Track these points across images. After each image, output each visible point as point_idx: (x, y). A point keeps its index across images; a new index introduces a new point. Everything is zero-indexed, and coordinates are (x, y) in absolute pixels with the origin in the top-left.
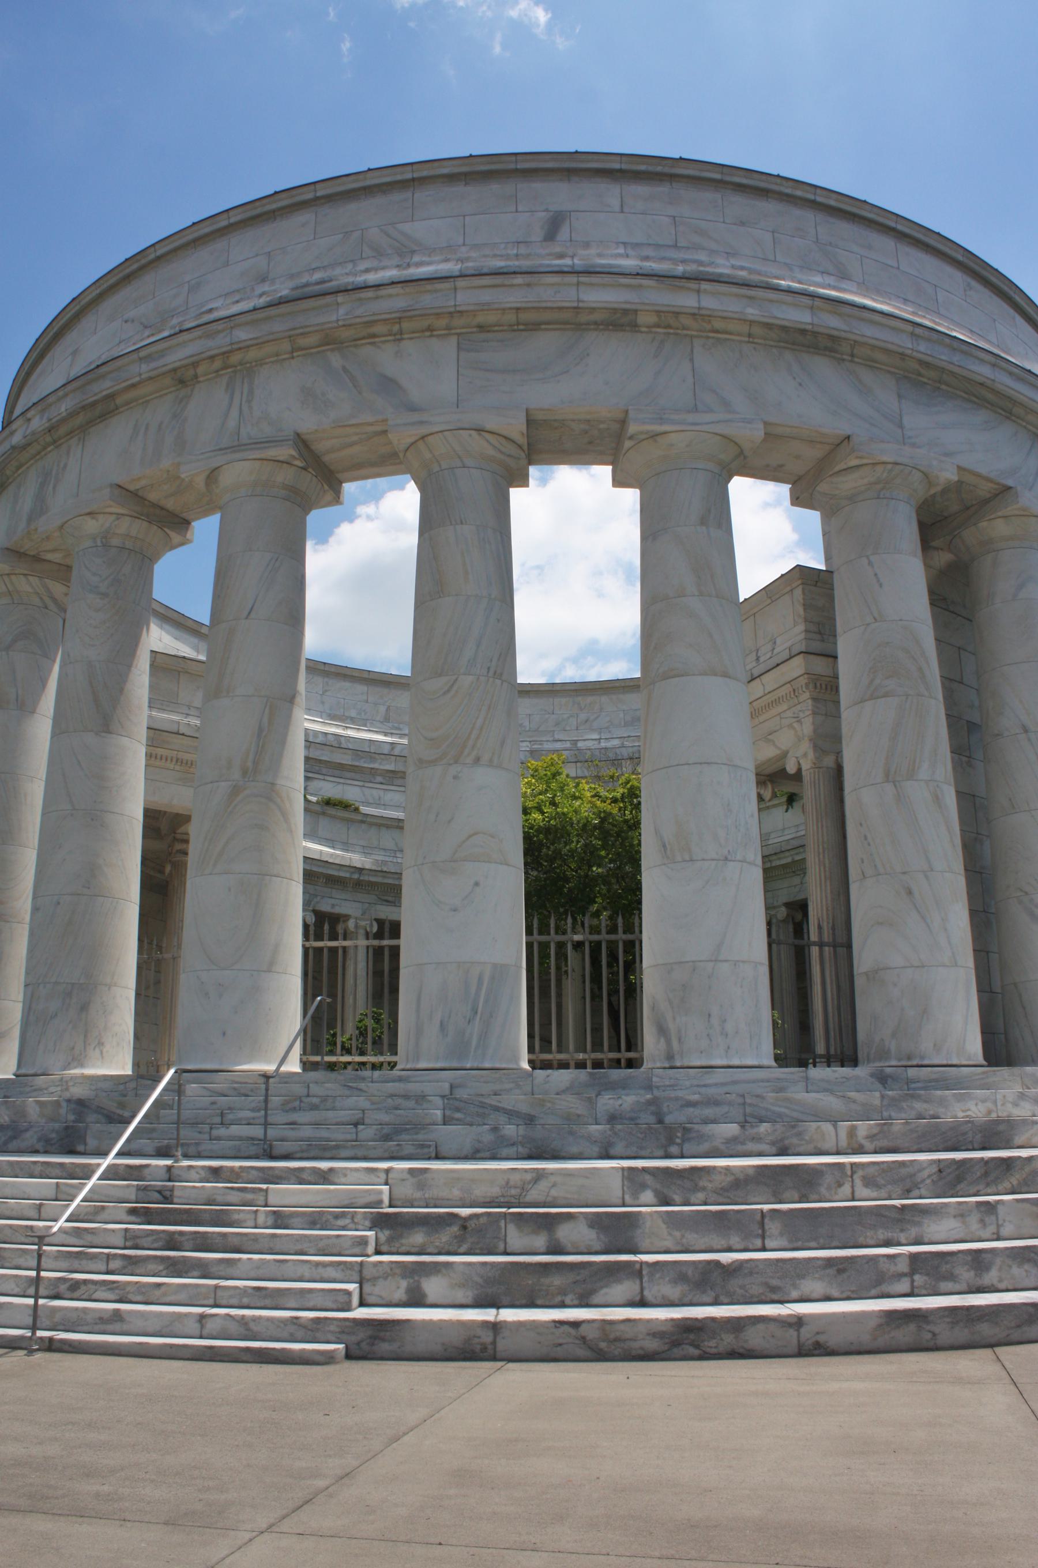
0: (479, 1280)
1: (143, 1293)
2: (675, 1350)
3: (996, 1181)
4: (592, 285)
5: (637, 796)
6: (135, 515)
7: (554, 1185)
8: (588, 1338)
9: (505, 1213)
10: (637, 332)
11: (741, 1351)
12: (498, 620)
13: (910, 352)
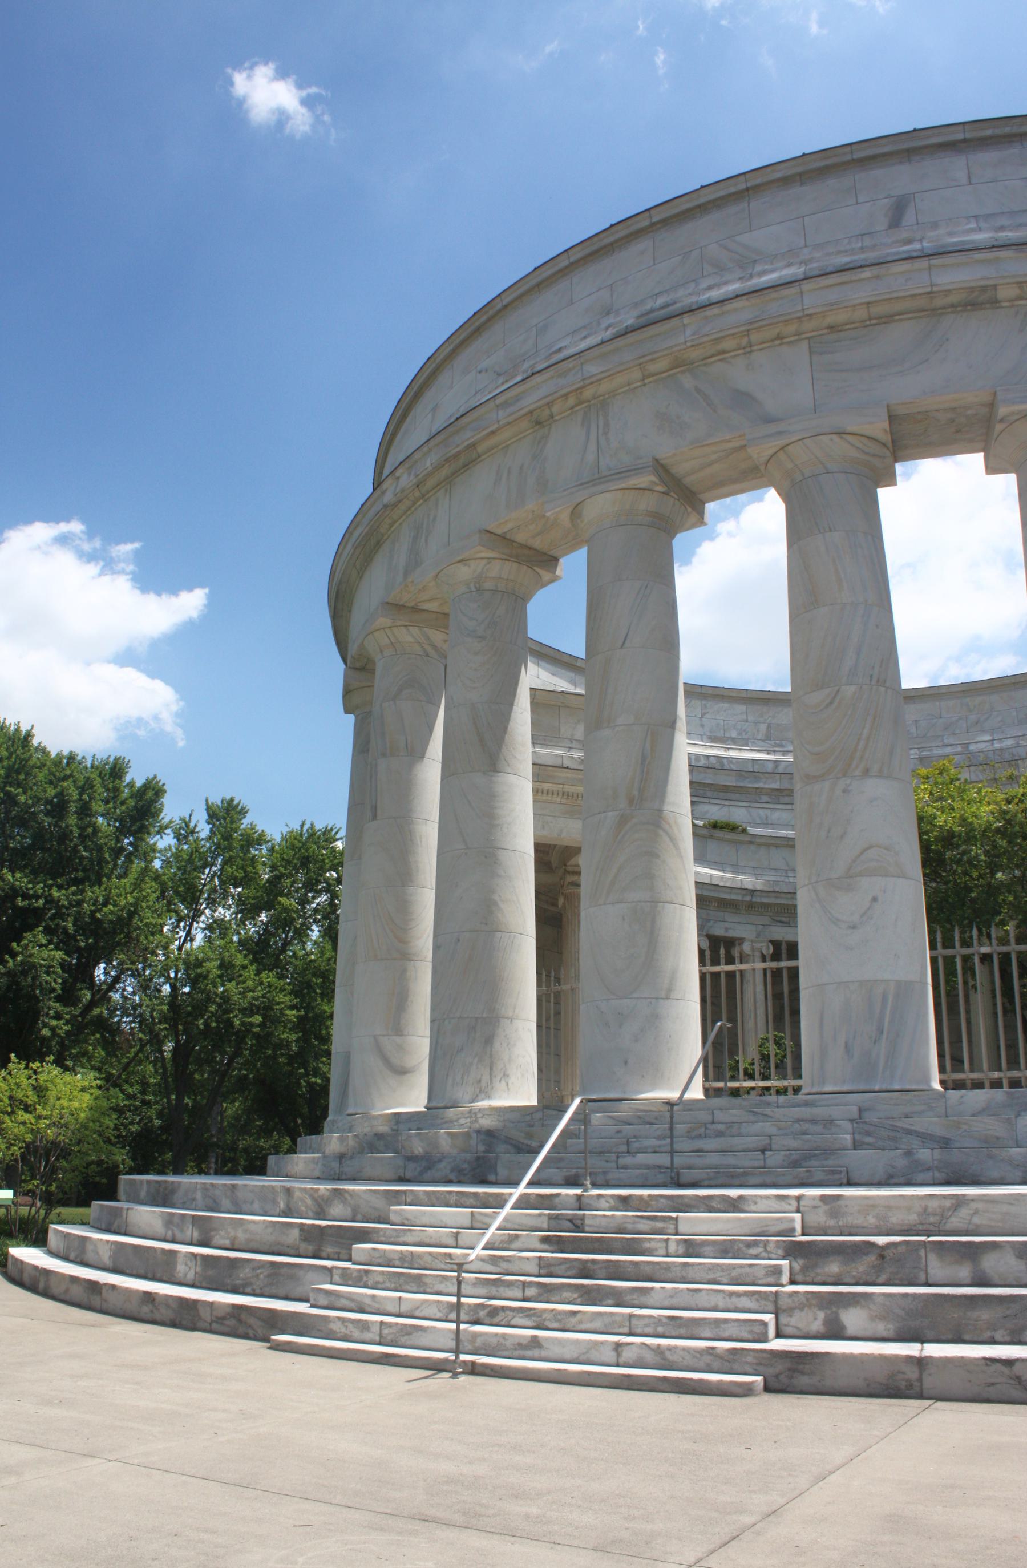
0: (902, 1313)
1: (559, 1321)
4: (943, 266)
6: (504, 557)
9: (924, 1242)
10: (998, 308)
12: (877, 626)
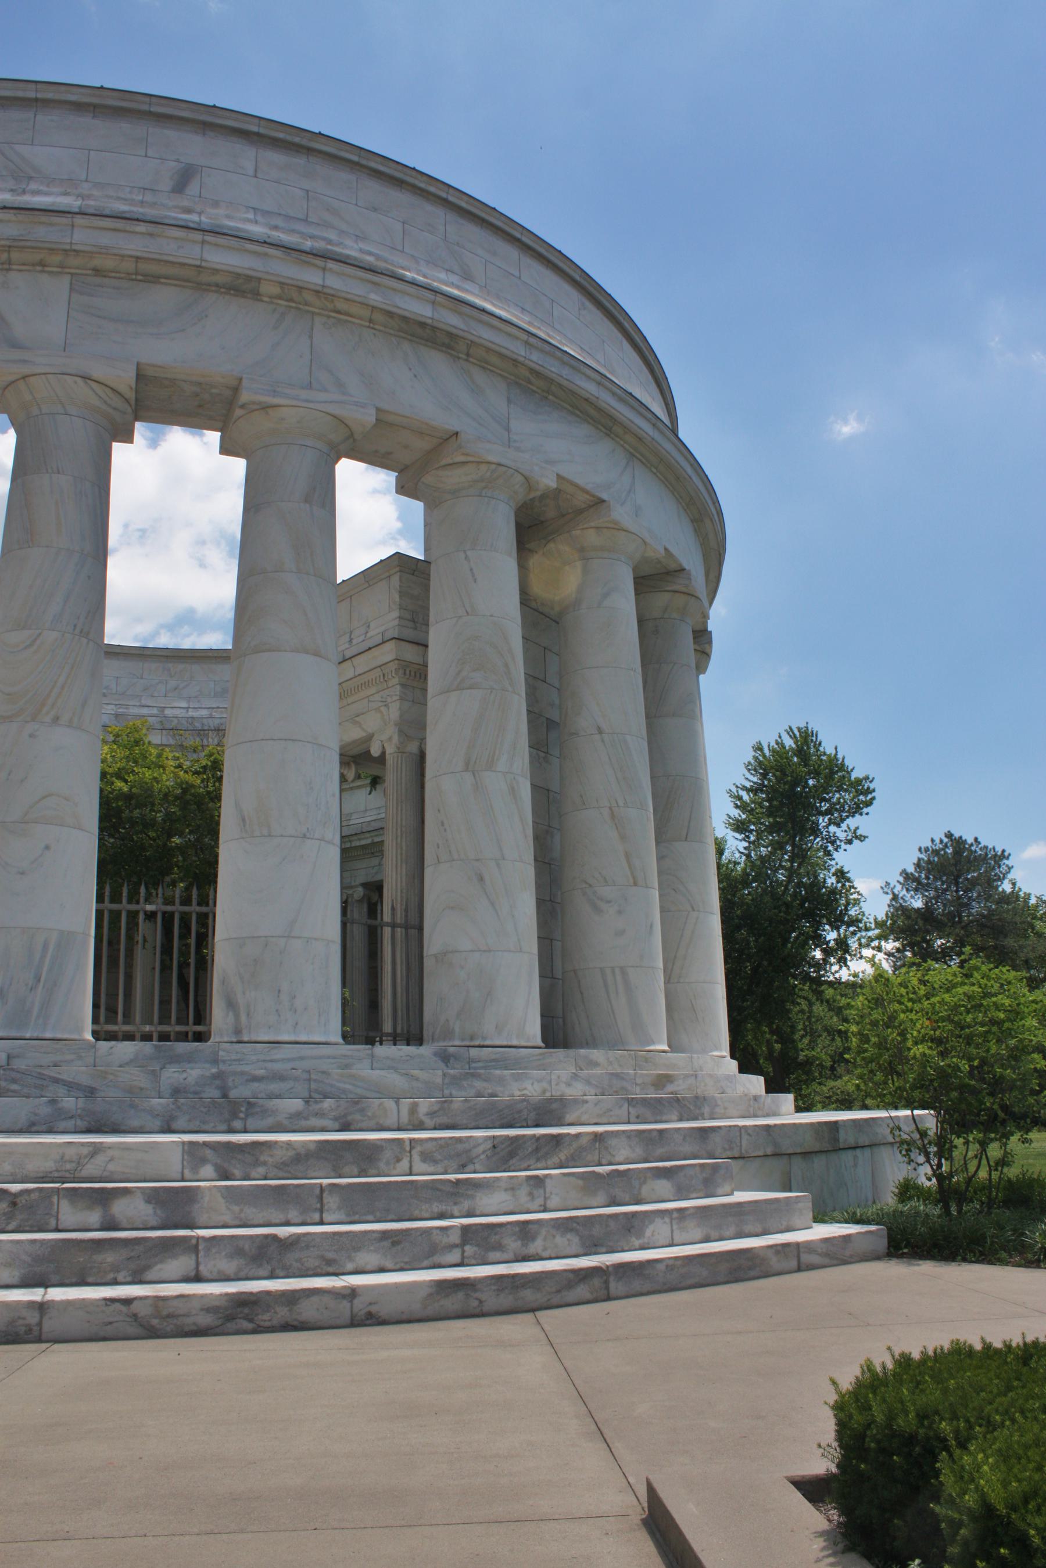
0: (28, 1259)
2: (229, 1325)
3: (546, 1156)
4: (216, 245)
5: (221, 770)
7: (112, 1159)
8: (140, 1316)
9: (58, 1189)
10: (259, 300)
11: (295, 1323)
13: (523, 359)
